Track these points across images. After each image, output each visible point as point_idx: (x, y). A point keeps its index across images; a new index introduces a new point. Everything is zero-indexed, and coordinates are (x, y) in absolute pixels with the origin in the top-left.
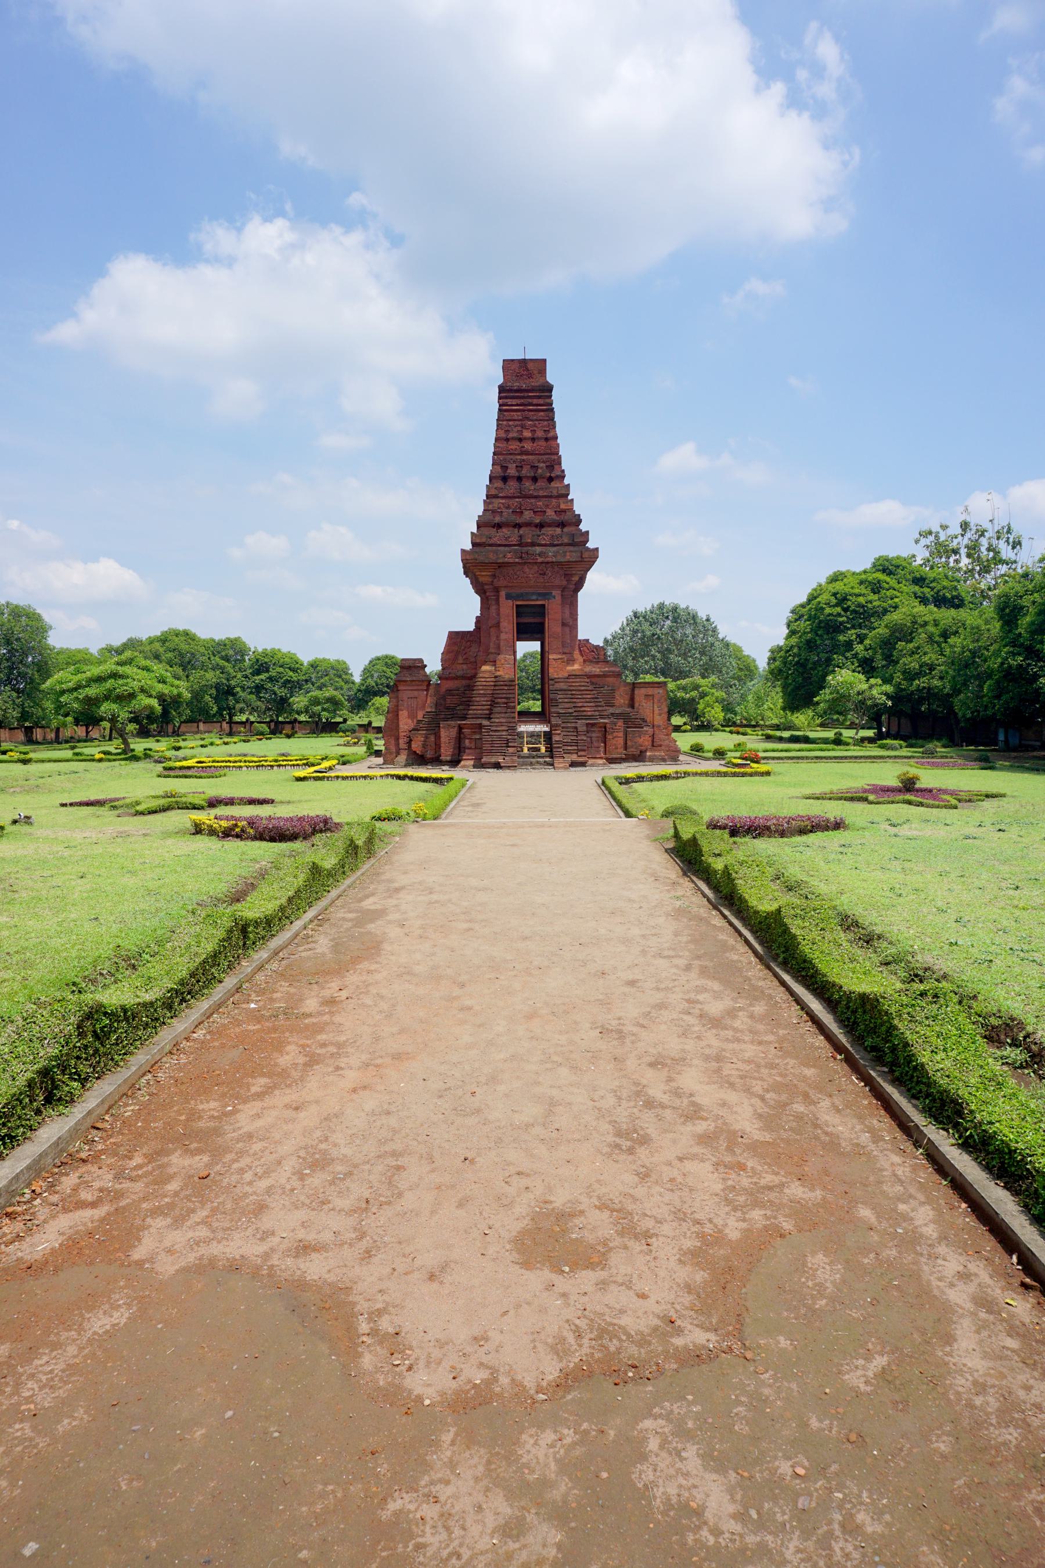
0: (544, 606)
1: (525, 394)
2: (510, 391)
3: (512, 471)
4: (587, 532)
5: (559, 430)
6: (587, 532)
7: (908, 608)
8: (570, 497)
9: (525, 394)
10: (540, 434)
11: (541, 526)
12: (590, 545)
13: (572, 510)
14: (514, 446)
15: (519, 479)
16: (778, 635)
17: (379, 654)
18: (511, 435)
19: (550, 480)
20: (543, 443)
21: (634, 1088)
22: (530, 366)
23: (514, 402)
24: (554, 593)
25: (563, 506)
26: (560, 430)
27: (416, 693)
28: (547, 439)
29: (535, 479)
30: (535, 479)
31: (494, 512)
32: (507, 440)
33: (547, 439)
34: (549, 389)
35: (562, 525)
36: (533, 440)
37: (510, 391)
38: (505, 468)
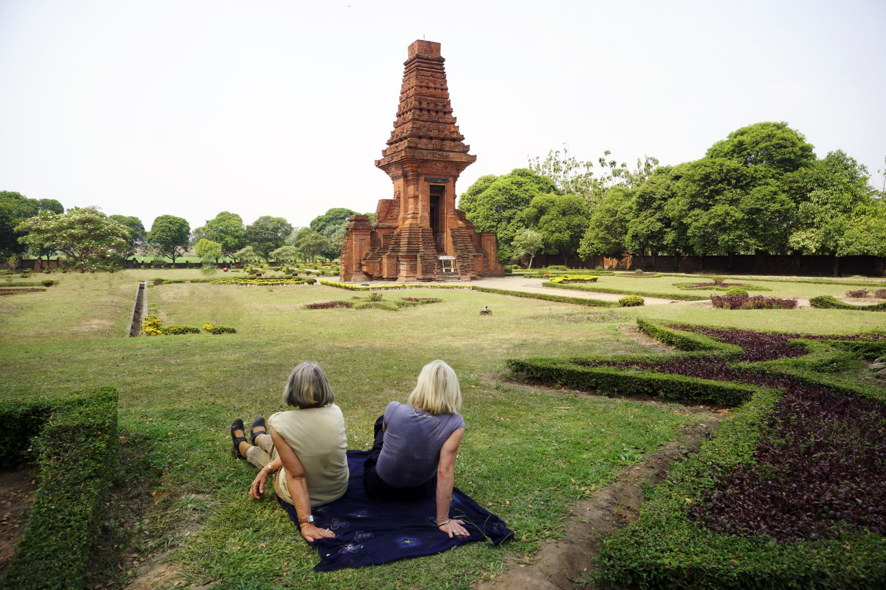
0: (444, 187)
1: (426, 64)
2: (422, 58)
3: (424, 105)
4: (468, 147)
5: (449, 85)
6: (468, 147)
7: (540, 198)
8: (456, 125)
9: (426, 64)
10: (438, 86)
11: (443, 139)
12: (470, 153)
13: (457, 132)
14: (425, 91)
15: (429, 111)
16: (203, 224)
17: (161, 215)
18: (423, 84)
19: (445, 113)
20: (440, 91)
21: (651, 472)
22: (432, 46)
23: (424, 65)
24: (450, 179)
25: (452, 129)
26: (449, 85)
27: (364, 237)
28: (442, 90)
29: (437, 112)
30: (437, 112)
31: (417, 129)
32: (421, 87)
33: (442, 90)
34: (442, 60)
35: (454, 140)
36: (435, 89)
37: (422, 58)
38: (420, 103)
